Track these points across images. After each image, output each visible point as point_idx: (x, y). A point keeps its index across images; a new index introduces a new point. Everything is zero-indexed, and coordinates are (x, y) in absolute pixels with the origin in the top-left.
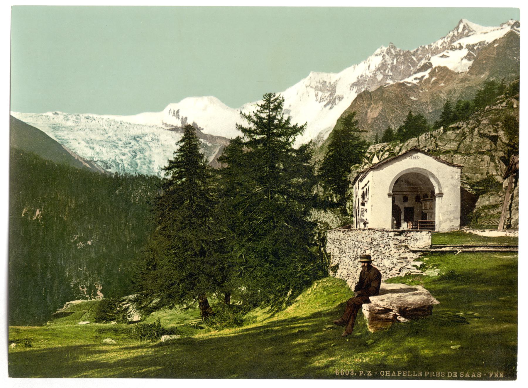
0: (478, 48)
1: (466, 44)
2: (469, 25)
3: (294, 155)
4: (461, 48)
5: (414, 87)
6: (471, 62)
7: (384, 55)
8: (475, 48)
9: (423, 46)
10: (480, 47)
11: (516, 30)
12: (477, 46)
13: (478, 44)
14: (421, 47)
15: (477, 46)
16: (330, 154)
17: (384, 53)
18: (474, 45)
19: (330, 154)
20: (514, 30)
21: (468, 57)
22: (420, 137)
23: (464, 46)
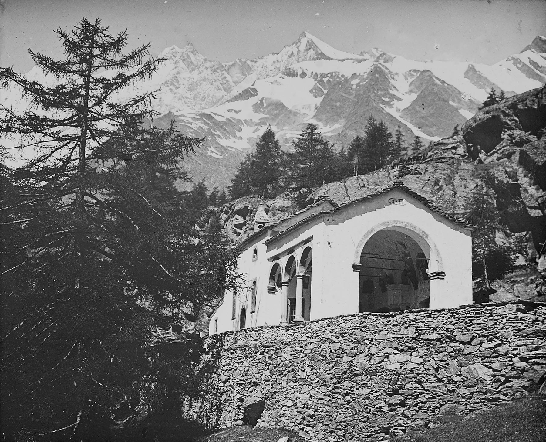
0: (329, 81)
1: (342, 74)
2: (314, 41)
3: (107, 249)
4: (303, 75)
5: (226, 124)
6: (320, 99)
7: (176, 61)
8: (325, 80)
9: (243, 60)
10: (331, 80)
11: (383, 66)
12: (328, 78)
13: (329, 75)
14: (240, 60)
15: (328, 78)
16: (507, 272)
17: (178, 58)
18: (323, 75)
19: (507, 272)
20: (379, 65)
21: (314, 91)
22: (348, 182)
23: (309, 73)
